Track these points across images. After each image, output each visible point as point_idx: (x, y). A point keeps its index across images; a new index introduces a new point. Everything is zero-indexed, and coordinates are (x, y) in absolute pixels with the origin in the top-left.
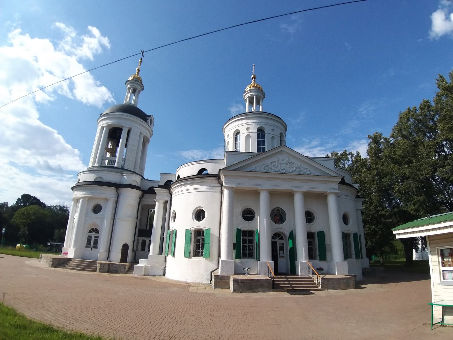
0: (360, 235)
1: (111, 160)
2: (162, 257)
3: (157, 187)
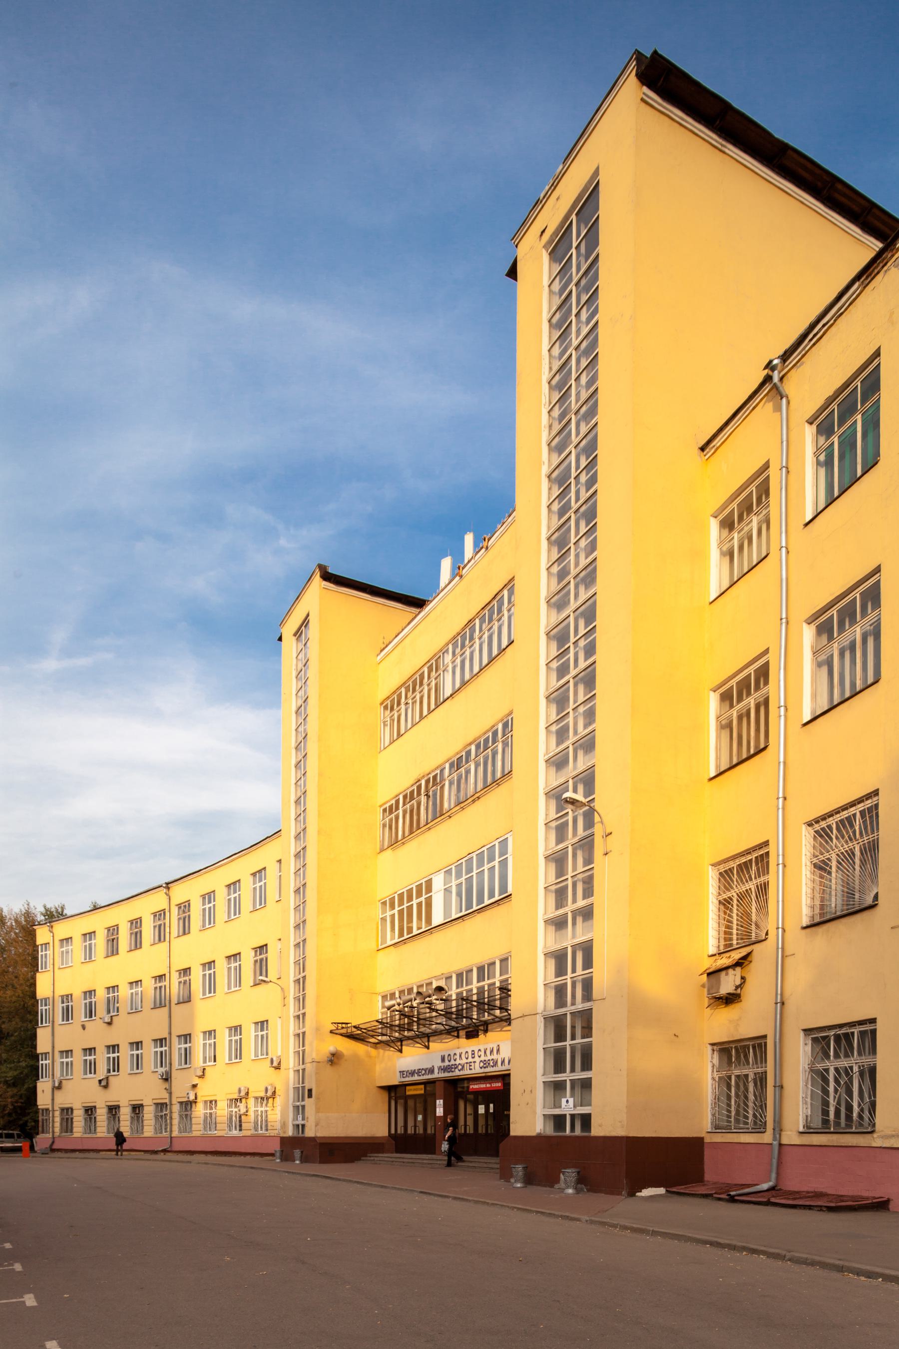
0: (804, 1030)
1: (101, 994)
2: (167, 943)
3: (779, 413)
